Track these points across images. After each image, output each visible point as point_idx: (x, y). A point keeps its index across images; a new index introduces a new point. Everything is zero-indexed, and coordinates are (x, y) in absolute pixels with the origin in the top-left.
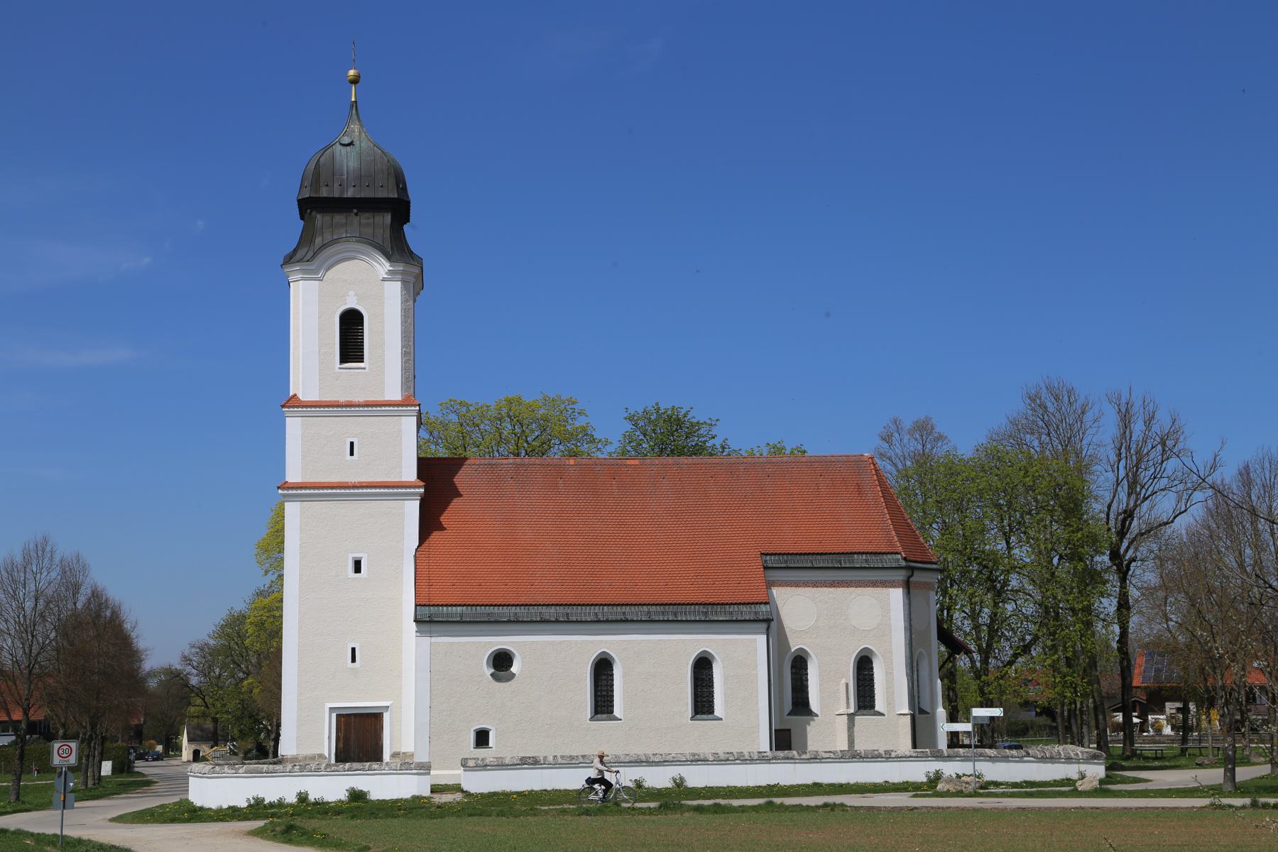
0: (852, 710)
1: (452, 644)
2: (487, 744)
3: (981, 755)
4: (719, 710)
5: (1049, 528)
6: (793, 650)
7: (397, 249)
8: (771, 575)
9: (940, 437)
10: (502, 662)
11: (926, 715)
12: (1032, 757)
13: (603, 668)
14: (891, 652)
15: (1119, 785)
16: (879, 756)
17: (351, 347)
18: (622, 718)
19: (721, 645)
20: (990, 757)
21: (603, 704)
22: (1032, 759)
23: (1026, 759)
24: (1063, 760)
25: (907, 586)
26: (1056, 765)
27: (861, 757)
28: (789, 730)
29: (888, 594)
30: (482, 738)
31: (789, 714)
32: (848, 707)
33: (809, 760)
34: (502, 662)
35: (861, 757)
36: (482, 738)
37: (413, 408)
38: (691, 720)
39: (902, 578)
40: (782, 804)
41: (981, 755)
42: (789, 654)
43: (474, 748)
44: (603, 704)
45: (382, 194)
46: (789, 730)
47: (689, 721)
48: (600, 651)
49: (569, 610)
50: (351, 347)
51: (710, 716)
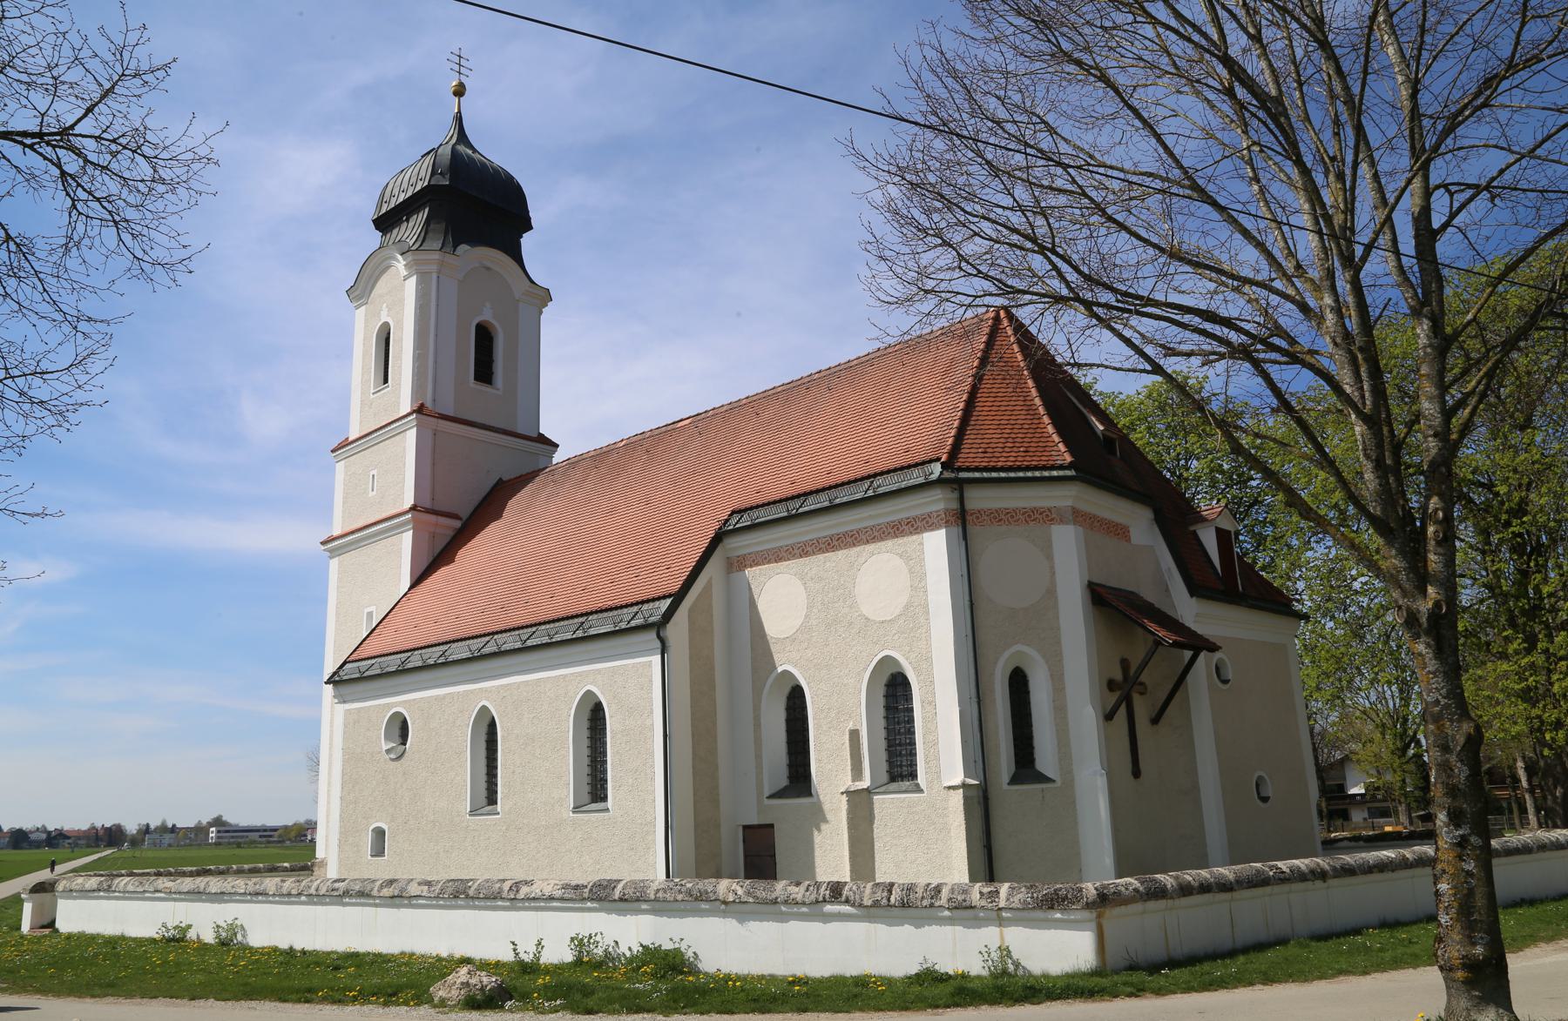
0: (866, 783)
1: (359, 710)
2: (913, 775)
3: (701, 897)
6: (780, 670)
8: (739, 544)
10: (400, 729)
12: (847, 901)
14: (929, 660)
16: (496, 896)
20: (725, 902)
22: (847, 909)
23: (829, 908)
24: (947, 913)
25: (961, 521)
26: (792, 923)
27: (467, 897)
28: (772, 826)
29: (922, 544)
32: (857, 773)
33: (317, 899)
34: (400, 729)
35: (467, 897)
37: (409, 418)
38: (573, 812)
39: (941, 506)
40: (227, 942)
41: (701, 897)
42: (773, 676)
43: (1008, 784)
46: (772, 826)
47: (571, 814)
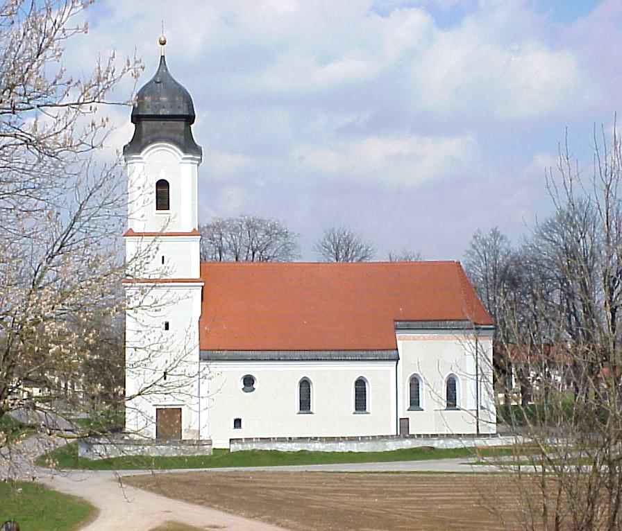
4: (313, 408)
5: (34, 277)
7: (189, 146)
9: (194, 229)
10: (249, 381)
11: (368, 415)
13: (305, 384)
15: (253, 470)
17: (163, 201)
18: (424, 409)
19: (370, 370)
21: (305, 405)
30: (238, 423)
31: (408, 410)
34: (249, 381)
36: (238, 423)
44: (305, 405)
45: (181, 112)
48: (413, 373)
49: (285, 353)
50: (163, 201)
51: (308, 411)
